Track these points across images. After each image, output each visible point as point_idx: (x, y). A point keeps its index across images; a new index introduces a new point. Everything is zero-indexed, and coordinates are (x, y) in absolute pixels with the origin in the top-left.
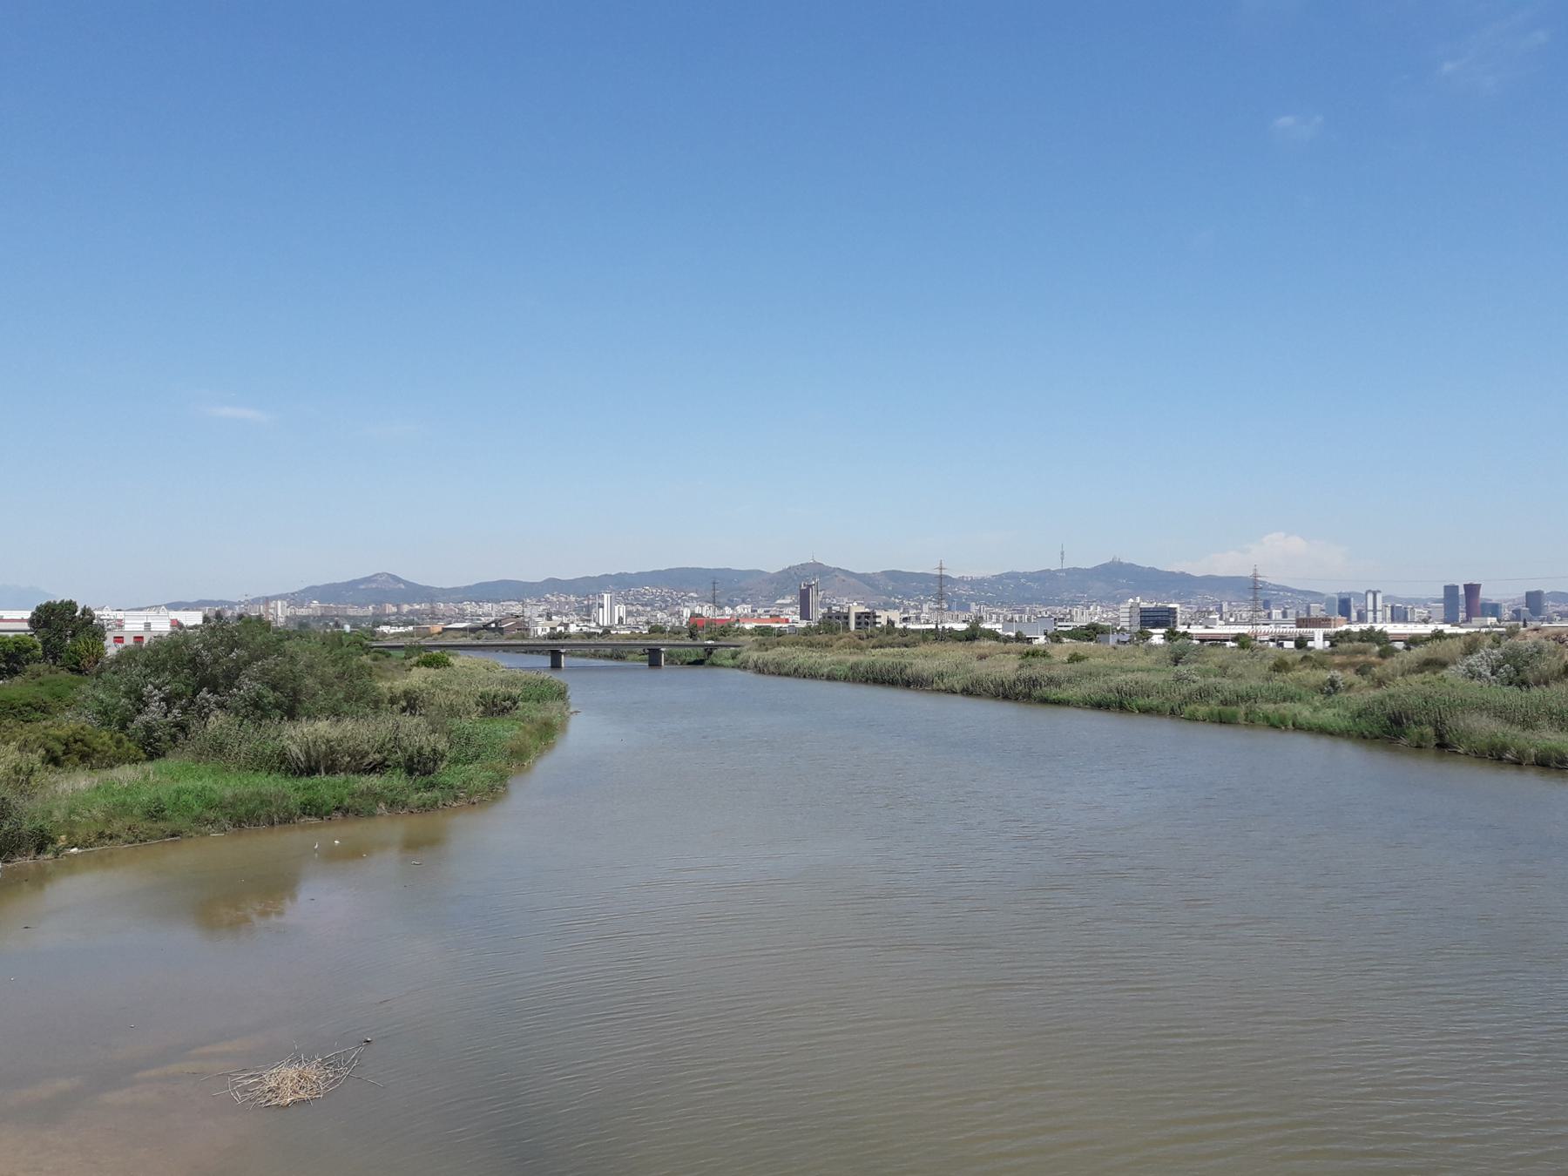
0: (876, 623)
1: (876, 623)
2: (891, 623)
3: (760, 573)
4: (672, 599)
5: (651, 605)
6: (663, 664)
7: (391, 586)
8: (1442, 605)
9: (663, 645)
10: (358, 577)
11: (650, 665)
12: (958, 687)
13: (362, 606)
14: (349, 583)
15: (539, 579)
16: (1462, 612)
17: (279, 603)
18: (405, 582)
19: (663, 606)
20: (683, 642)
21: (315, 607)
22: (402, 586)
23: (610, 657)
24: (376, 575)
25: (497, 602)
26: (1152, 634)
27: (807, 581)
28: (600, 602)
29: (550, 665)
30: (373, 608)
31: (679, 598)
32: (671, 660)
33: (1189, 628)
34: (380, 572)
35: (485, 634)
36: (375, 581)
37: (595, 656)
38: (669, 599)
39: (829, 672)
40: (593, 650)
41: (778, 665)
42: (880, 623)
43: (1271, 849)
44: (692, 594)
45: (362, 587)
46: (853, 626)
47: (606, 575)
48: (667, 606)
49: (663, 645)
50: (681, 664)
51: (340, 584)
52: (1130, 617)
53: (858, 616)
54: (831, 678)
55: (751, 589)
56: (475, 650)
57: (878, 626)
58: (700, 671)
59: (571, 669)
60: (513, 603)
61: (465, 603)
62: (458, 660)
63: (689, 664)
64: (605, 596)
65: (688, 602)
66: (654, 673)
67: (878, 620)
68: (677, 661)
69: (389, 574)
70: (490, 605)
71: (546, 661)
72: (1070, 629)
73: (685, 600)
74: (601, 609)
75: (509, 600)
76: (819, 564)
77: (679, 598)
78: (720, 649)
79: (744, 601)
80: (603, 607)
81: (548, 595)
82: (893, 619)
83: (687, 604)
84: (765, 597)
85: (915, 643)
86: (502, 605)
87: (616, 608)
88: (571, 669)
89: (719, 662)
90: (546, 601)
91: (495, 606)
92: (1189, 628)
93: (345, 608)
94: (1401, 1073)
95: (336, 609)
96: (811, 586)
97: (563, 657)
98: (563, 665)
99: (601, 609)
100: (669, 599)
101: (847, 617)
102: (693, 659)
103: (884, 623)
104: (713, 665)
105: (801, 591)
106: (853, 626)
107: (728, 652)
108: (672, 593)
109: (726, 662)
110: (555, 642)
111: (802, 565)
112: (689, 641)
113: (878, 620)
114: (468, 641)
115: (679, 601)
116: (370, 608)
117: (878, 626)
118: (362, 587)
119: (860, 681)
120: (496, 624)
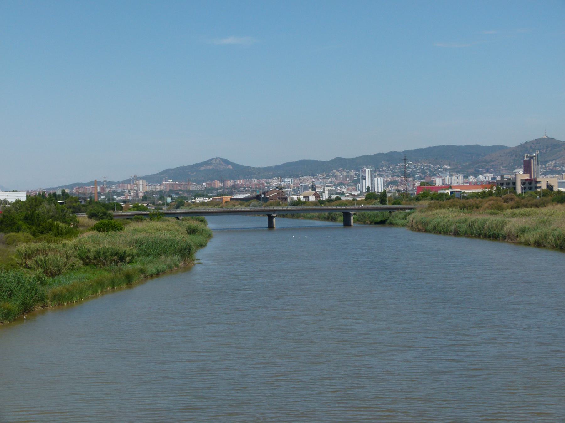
0: (537, 188)
1: (537, 188)
2: (550, 187)
3: (501, 148)
4: (429, 170)
7: (222, 167)
9: (352, 210)
12: (532, 240)
13: (199, 182)
14: (192, 166)
17: (141, 182)
19: (423, 176)
21: (166, 184)
22: (231, 167)
23: (327, 219)
24: (212, 159)
25: (297, 176)
26: (77, 217)
27: (529, 153)
28: (363, 175)
29: (267, 226)
30: (206, 184)
31: (436, 170)
32: (362, 221)
34: (215, 157)
35: (254, 202)
36: (211, 164)
38: (427, 171)
39: (455, 229)
40: (327, 214)
42: (540, 187)
43: (347, 318)
44: (446, 167)
45: (202, 168)
46: (519, 190)
48: (425, 176)
49: (352, 210)
50: (371, 224)
51: (187, 166)
53: (523, 182)
54: (456, 233)
55: (493, 161)
56: (241, 215)
57: (539, 190)
58: (380, 230)
59: (282, 230)
60: (308, 177)
61: (274, 178)
63: (376, 223)
64: (367, 170)
65: (442, 173)
66: (348, 231)
67: (538, 185)
69: (221, 159)
71: (264, 221)
73: (440, 171)
74: (364, 181)
76: (551, 139)
77: (436, 170)
79: (488, 171)
80: (365, 179)
82: (552, 184)
83: (441, 175)
84: (506, 167)
85: (544, 204)
87: (376, 179)
88: (282, 230)
90: (333, 175)
94: (256, 396)
95: (180, 185)
96: (532, 157)
98: (275, 226)
100: (427, 171)
101: (514, 184)
103: (544, 187)
104: (391, 224)
105: (525, 161)
106: (519, 190)
107: (401, 214)
109: (399, 222)
110: (295, 208)
111: (536, 140)
112: (379, 206)
113: (538, 185)
115: (436, 172)
116: (204, 184)
117: (539, 190)
118: (202, 168)
119: (476, 236)
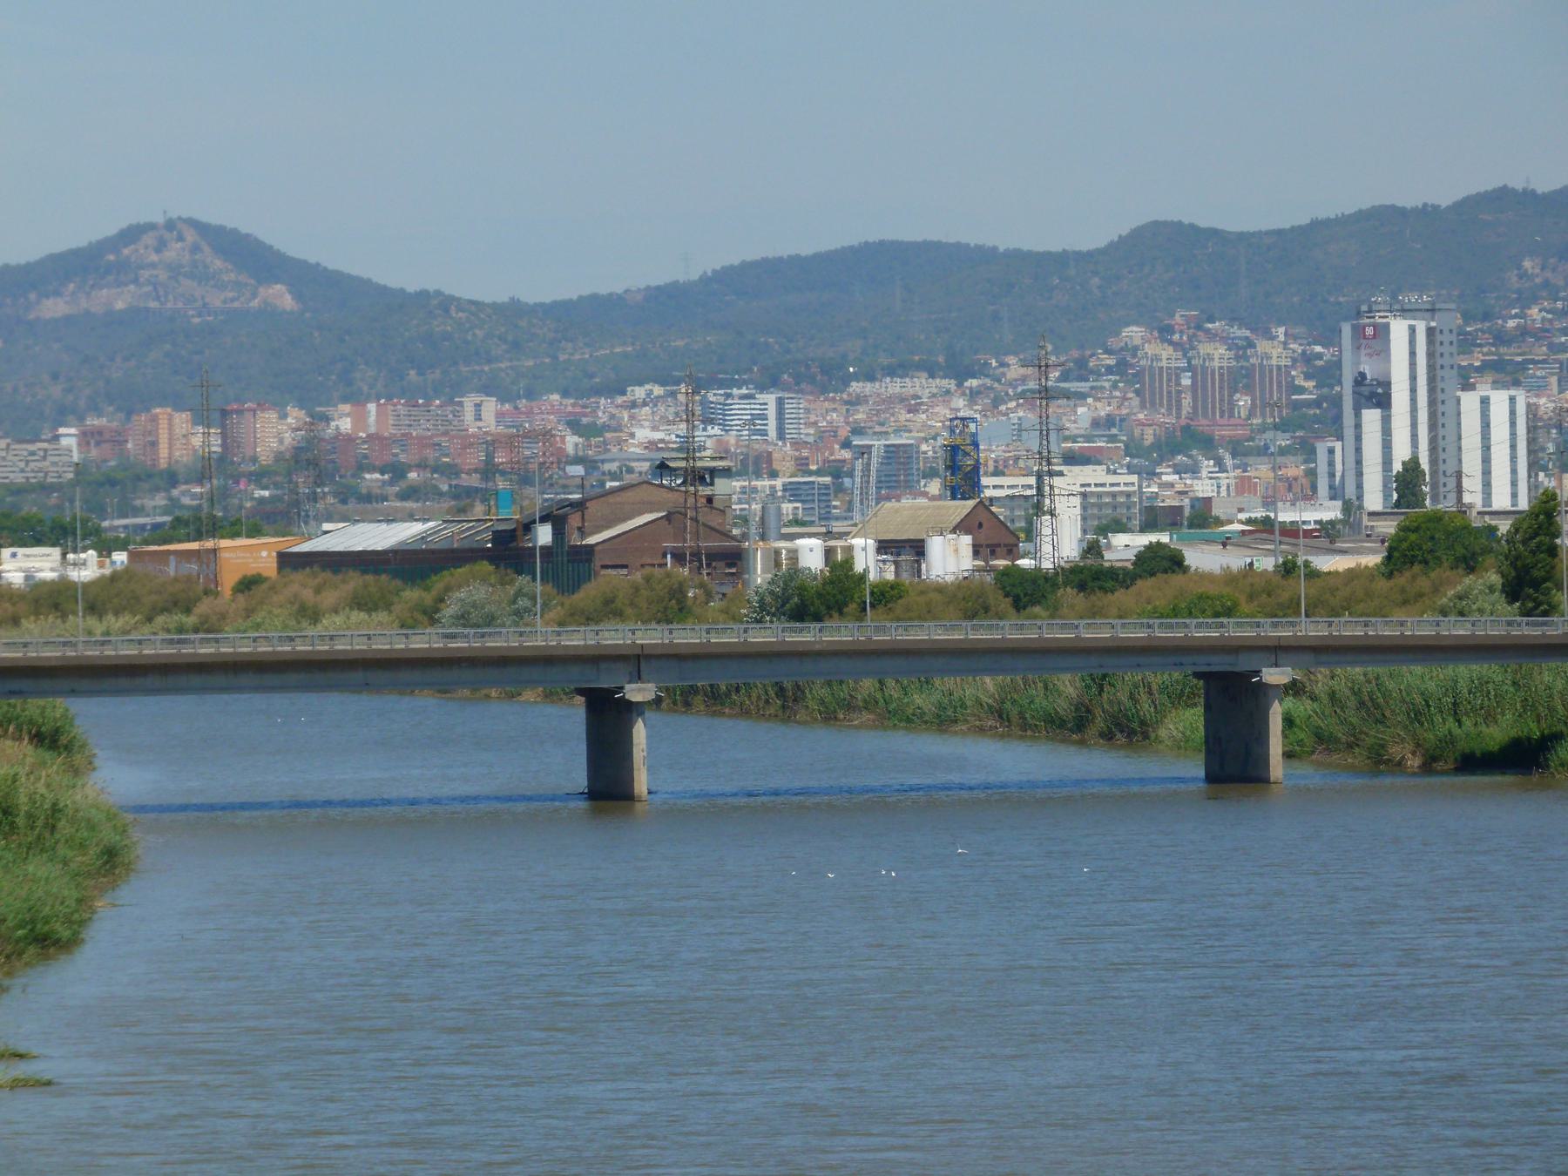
7: (216, 300)
8: (372, 407)
9: (1278, 651)
11: (1212, 778)
16: (360, 419)
18: (303, 276)
20: (1460, 630)
22: (281, 297)
24: (132, 234)
45: (53, 308)
47: (1501, 197)
49: (1278, 651)
50: (1428, 768)
52: (694, 437)
56: (366, 687)
60: (920, 385)
63: (1473, 763)
64: (1399, 329)
70: (770, 399)
74: (1371, 417)
75: (899, 369)
80: (1382, 401)
87: (1469, 403)
90: (1121, 368)
91: (796, 405)
92: (1245, 471)
97: (640, 732)
98: (642, 782)
99: (1371, 417)
102: (1496, 735)
116: (69, 437)
118: (53, 308)
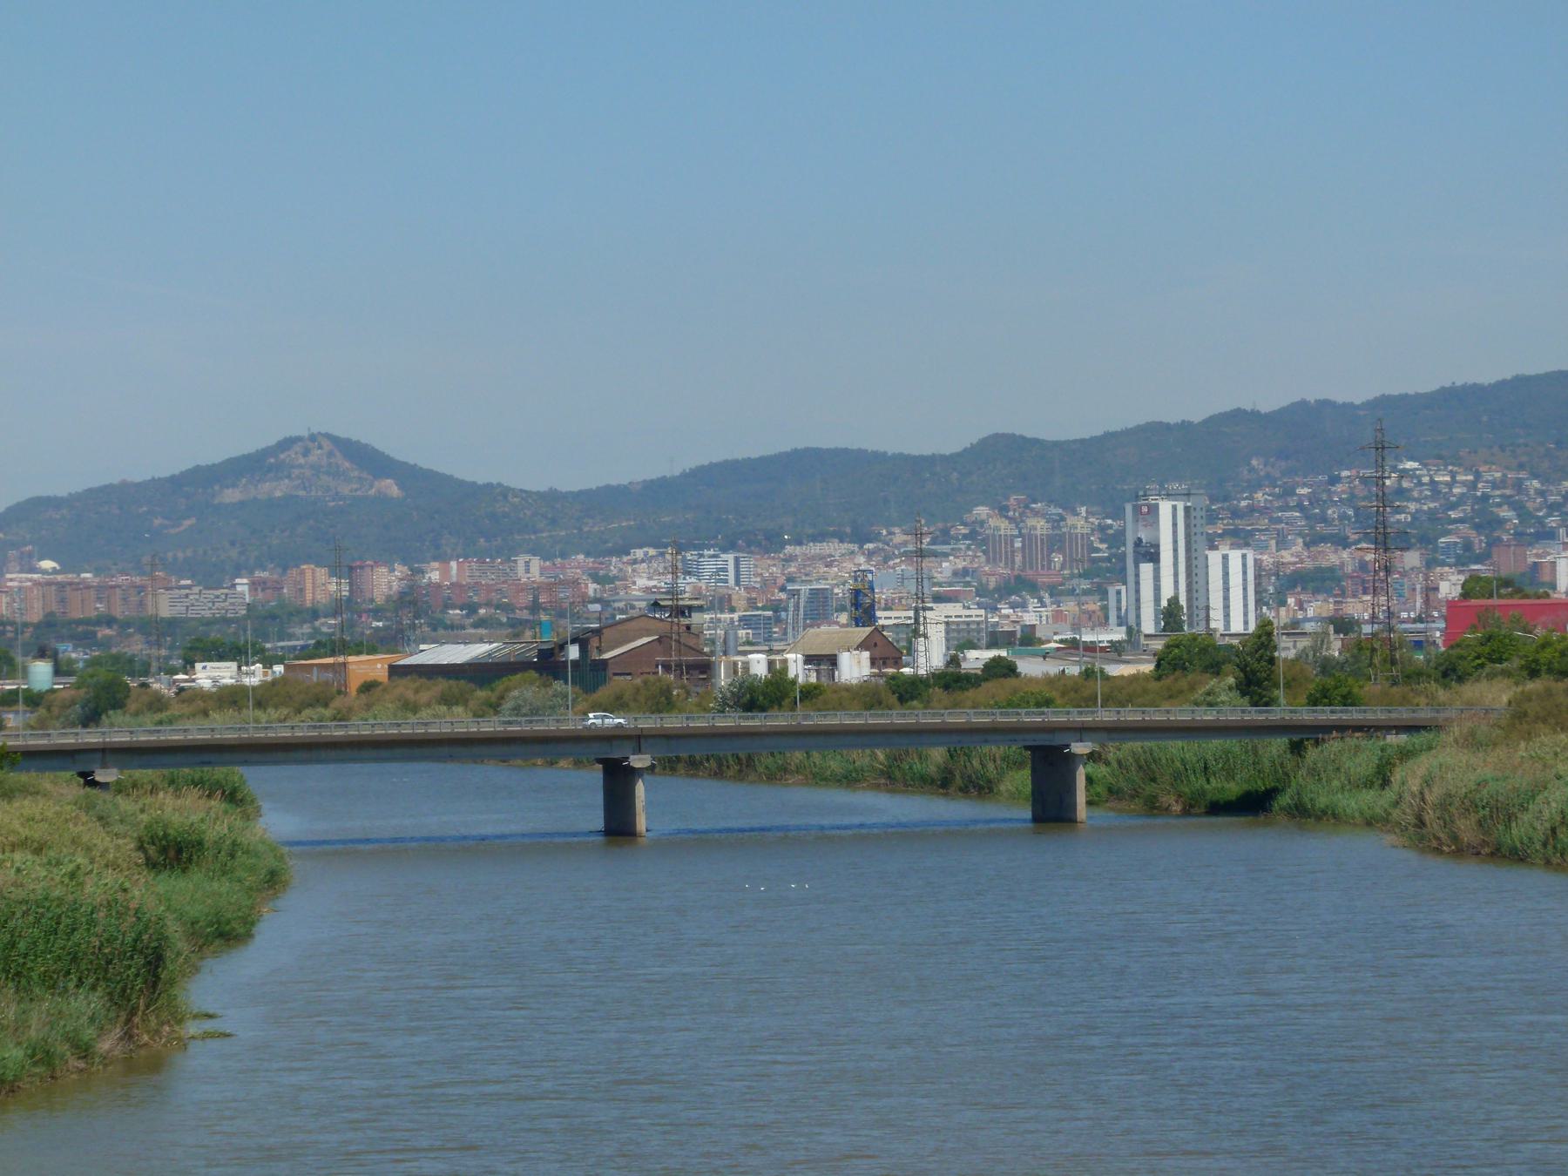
4: (1519, 508)
5: (1426, 541)
6: (1082, 811)
7: (345, 490)
9: (1082, 731)
10: (212, 453)
11: (1037, 819)
13: (213, 576)
14: (176, 482)
15: (951, 442)
18: (407, 474)
20: (1209, 716)
22: (390, 487)
23: (943, 783)
24: (287, 444)
25: (769, 543)
29: (599, 824)
31: (1552, 508)
33: (1059, 606)
35: (525, 690)
37: (892, 779)
38: (1505, 513)
41: (1501, 812)
45: (231, 496)
47: (1237, 416)
48: (1494, 543)
49: (1082, 731)
60: (833, 548)
62: (1198, 786)
63: (1218, 808)
64: (1165, 508)
68: (1168, 799)
70: (730, 557)
72: (200, 616)
74: (1146, 569)
75: (815, 538)
78: (1333, 745)
80: (1153, 556)
81: (982, 511)
86: (790, 559)
87: (1214, 558)
89: (1322, 801)
90: (972, 536)
91: (748, 564)
93: (141, 589)
95: (103, 591)
98: (642, 823)
100: (1505, 513)
104: (1301, 813)
107: (1361, 756)
108: (1519, 486)
112: (1236, 710)
114: (460, 721)
116: (242, 585)
118: (231, 496)
120: (584, 650)
